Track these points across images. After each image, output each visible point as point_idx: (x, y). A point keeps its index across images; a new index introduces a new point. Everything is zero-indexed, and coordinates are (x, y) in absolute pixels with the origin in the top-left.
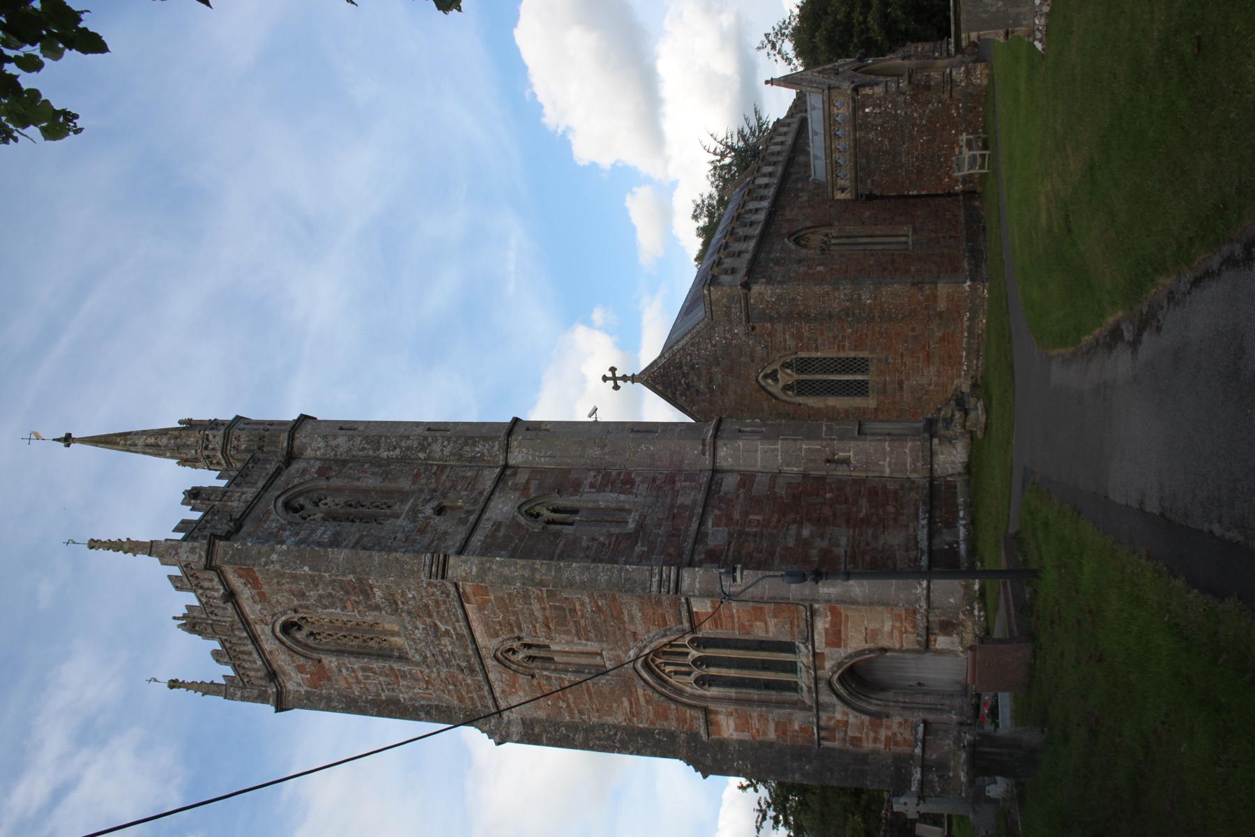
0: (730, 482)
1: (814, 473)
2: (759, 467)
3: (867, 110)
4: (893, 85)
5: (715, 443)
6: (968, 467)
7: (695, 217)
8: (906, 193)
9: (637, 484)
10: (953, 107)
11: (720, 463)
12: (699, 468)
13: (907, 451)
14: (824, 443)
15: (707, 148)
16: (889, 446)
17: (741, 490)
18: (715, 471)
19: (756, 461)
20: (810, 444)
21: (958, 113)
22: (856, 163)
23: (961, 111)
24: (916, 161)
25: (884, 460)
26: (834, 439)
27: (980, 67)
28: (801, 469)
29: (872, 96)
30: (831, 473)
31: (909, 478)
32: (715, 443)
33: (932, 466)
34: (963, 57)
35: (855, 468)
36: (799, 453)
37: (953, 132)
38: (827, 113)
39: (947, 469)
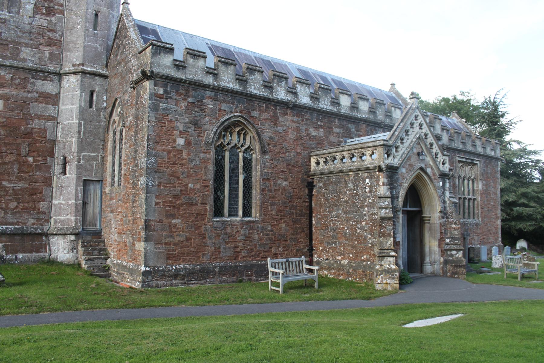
0: (49, 87)
1: (57, 148)
2: (62, 107)
3: (367, 180)
4: (386, 203)
5: (79, 72)
6: (52, 262)
7: (462, 93)
8: (314, 215)
9: (48, 18)
10: (368, 257)
11: (66, 78)
12: (64, 63)
13: (69, 217)
14: (75, 155)
15: (498, 93)
16: (72, 203)
17: (36, 95)
18: (60, 76)
19: (66, 105)
20: (75, 144)
21: (363, 261)
22: (332, 173)
23: (365, 263)
24: (333, 223)
25: (63, 200)
26: (79, 162)
27: (395, 283)
28: (60, 139)
29: (378, 184)
30: (56, 160)
31: (51, 218)
32: (79, 72)
33: (56, 234)
34: (440, 263)
35: (59, 178)
36: (70, 136)
37: (351, 256)
38: (366, 145)
39: (54, 246)
